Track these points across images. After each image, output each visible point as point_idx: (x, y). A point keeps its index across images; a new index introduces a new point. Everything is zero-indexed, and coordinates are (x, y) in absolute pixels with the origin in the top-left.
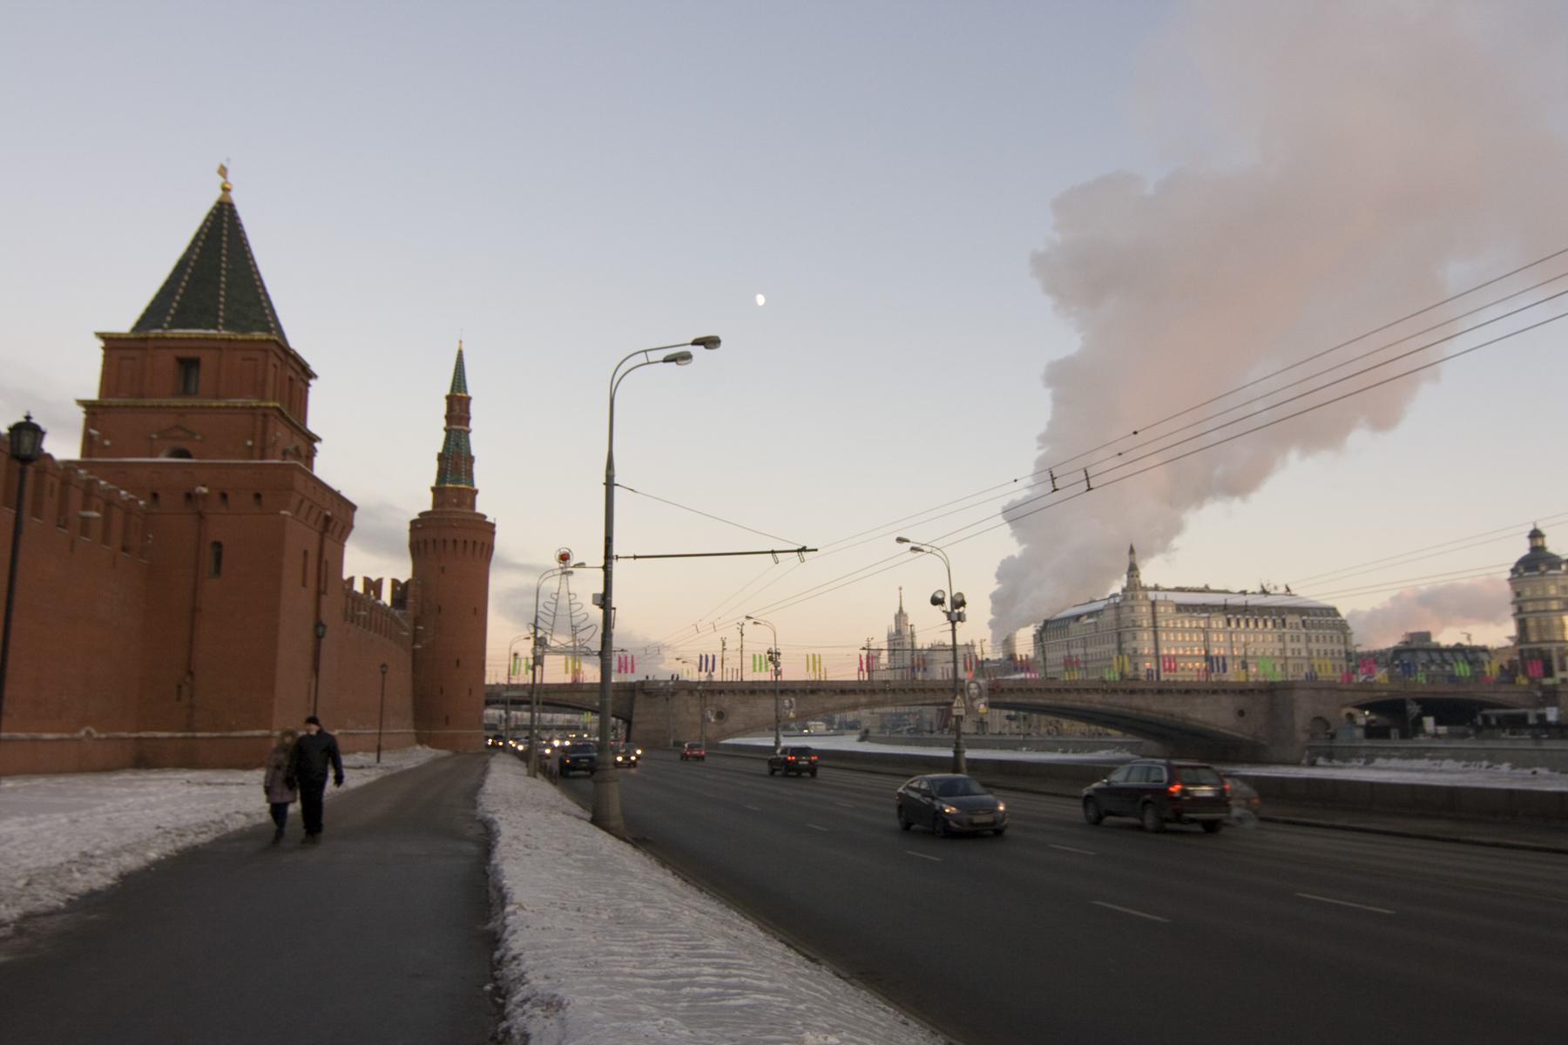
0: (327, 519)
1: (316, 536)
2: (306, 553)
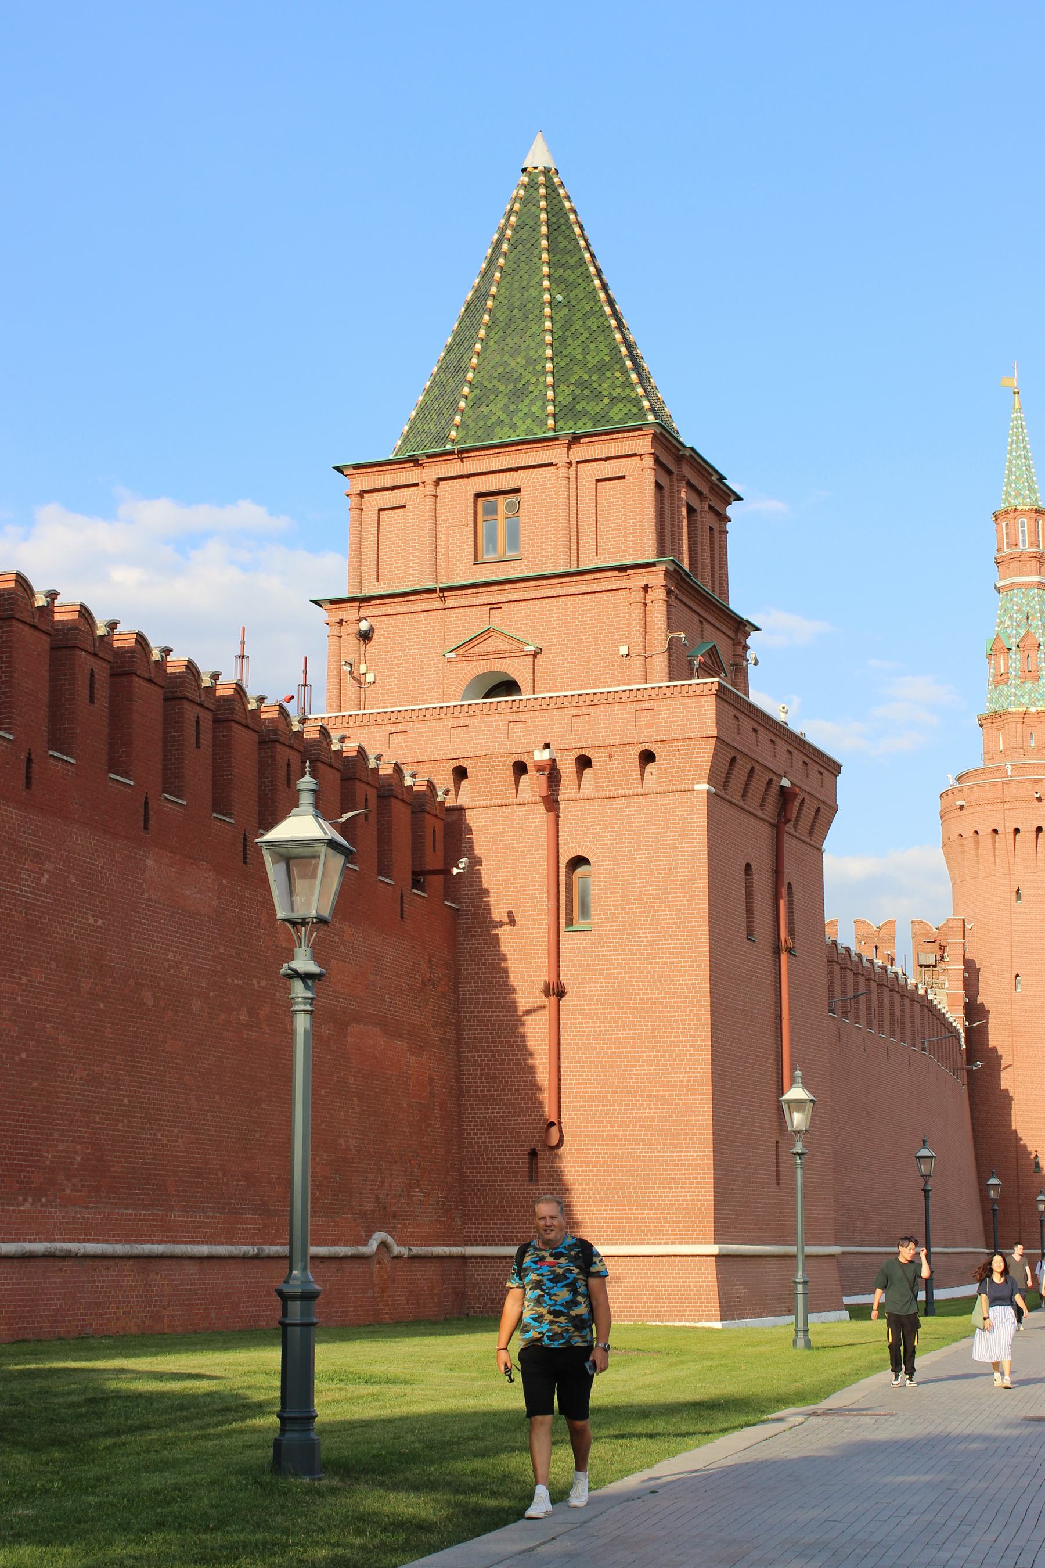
0: (785, 796)
1: (765, 833)
2: (748, 867)
